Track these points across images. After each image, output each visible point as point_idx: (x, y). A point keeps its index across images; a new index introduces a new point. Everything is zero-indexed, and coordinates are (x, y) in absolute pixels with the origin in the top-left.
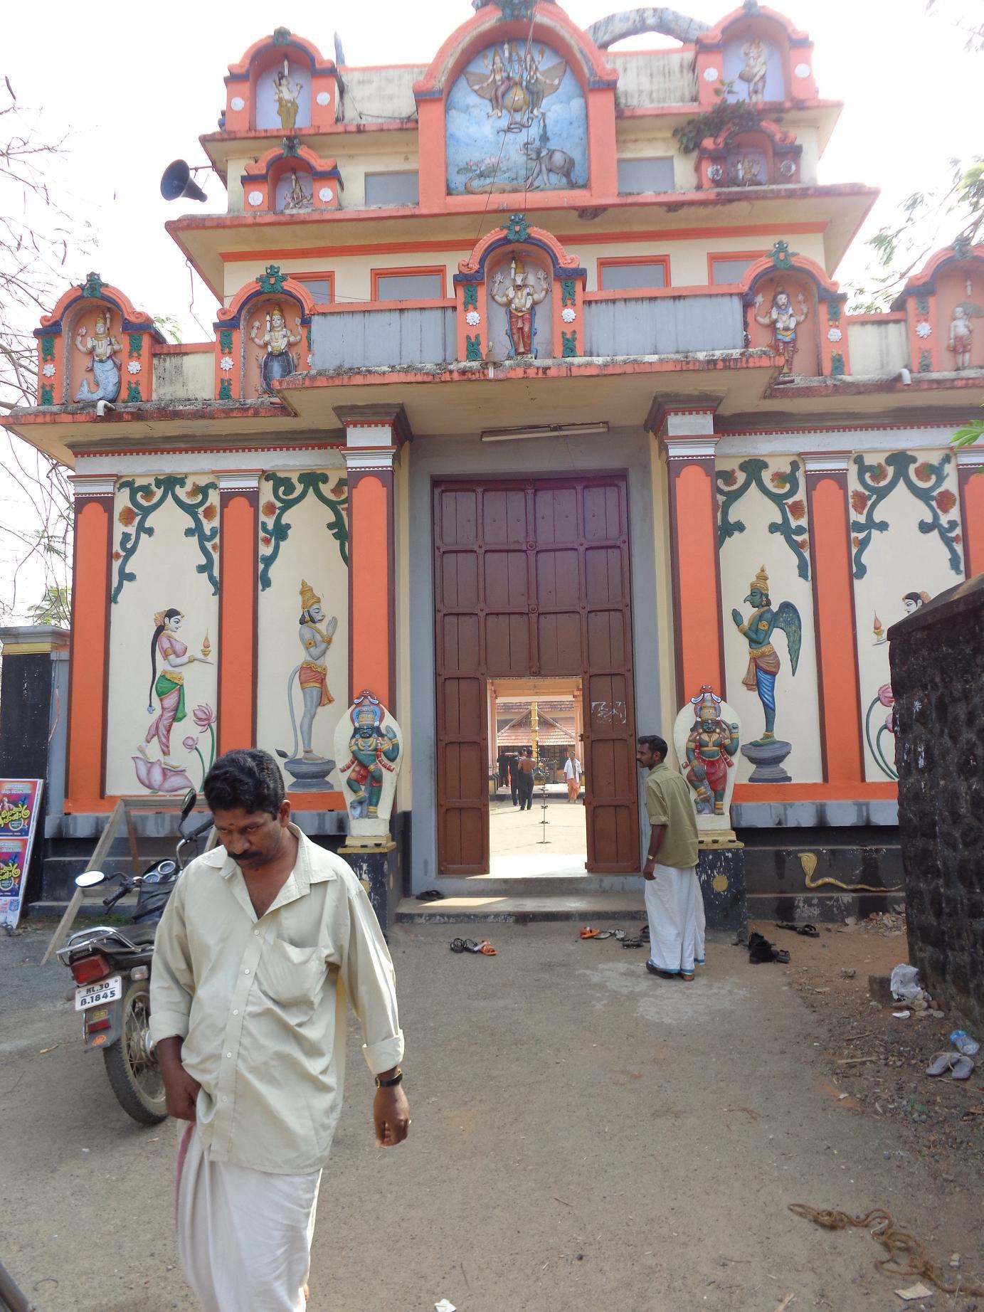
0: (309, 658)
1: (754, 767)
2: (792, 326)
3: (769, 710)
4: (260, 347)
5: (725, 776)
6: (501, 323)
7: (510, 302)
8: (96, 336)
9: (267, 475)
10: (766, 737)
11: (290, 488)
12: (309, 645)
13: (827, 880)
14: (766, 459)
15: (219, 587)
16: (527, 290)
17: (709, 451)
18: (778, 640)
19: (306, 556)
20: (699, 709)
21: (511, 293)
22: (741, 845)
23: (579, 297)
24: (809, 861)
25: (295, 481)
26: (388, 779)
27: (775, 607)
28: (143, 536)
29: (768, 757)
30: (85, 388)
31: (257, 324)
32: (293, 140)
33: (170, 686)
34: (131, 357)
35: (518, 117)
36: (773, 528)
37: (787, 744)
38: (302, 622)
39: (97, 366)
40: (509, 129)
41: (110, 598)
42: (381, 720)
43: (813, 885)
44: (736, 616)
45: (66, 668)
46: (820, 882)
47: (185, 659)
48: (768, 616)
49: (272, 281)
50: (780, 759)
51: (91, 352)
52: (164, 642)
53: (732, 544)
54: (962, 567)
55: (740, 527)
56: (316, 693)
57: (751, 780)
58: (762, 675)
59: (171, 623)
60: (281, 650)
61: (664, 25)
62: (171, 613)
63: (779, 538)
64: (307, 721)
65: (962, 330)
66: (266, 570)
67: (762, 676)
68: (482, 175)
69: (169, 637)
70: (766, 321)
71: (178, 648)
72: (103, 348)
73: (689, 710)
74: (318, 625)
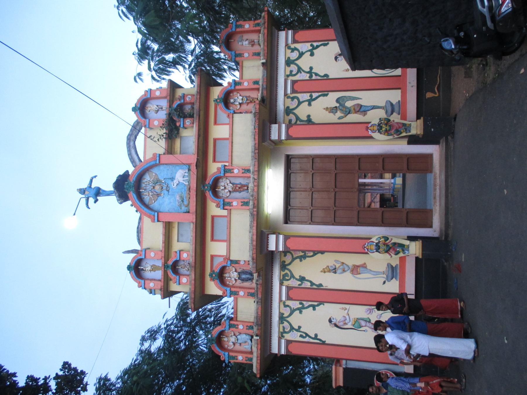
0: (349, 271)
1: (394, 114)
2: (241, 98)
3: (374, 107)
4: (236, 282)
5: (397, 123)
6: (236, 195)
7: (230, 192)
8: (228, 341)
9: (281, 284)
10: (383, 109)
11: (286, 275)
12: (344, 271)
13: (436, 89)
14: (286, 107)
15: (321, 303)
16: (226, 186)
17: (283, 126)
18: (349, 104)
19: (312, 270)
20: (373, 131)
21: (227, 191)
22: (422, 118)
23: (230, 168)
24: (429, 95)
25: (284, 273)
26: (395, 240)
27: (338, 105)
28: (301, 330)
29: (391, 108)
30: (247, 347)
31: (228, 283)
32: (165, 266)
33: (357, 323)
34: (237, 328)
35: (164, 188)
36: (310, 105)
37: (387, 102)
38: (335, 273)
39: (239, 342)
40: (168, 191)
41: (323, 343)
42: (373, 242)
43: (437, 94)
44: (339, 118)
45: (348, 362)
46: (436, 91)
47: (347, 317)
48: (341, 108)
49: (214, 275)
50: (392, 104)
51: (234, 344)
52: (340, 324)
53: (314, 119)
54: (326, 42)
55: (309, 116)
56: (362, 269)
57: (399, 114)
58: (362, 110)
59: (334, 321)
60: (345, 281)
61: (131, 138)
62: (330, 321)
63: (313, 103)
64: (372, 273)
65: (247, 42)
66: (316, 285)
67: (361, 109)
68: (183, 201)
69: (339, 322)
70: (239, 106)
71: (343, 319)
72: (233, 339)
73: (373, 135)
74: (337, 267)
